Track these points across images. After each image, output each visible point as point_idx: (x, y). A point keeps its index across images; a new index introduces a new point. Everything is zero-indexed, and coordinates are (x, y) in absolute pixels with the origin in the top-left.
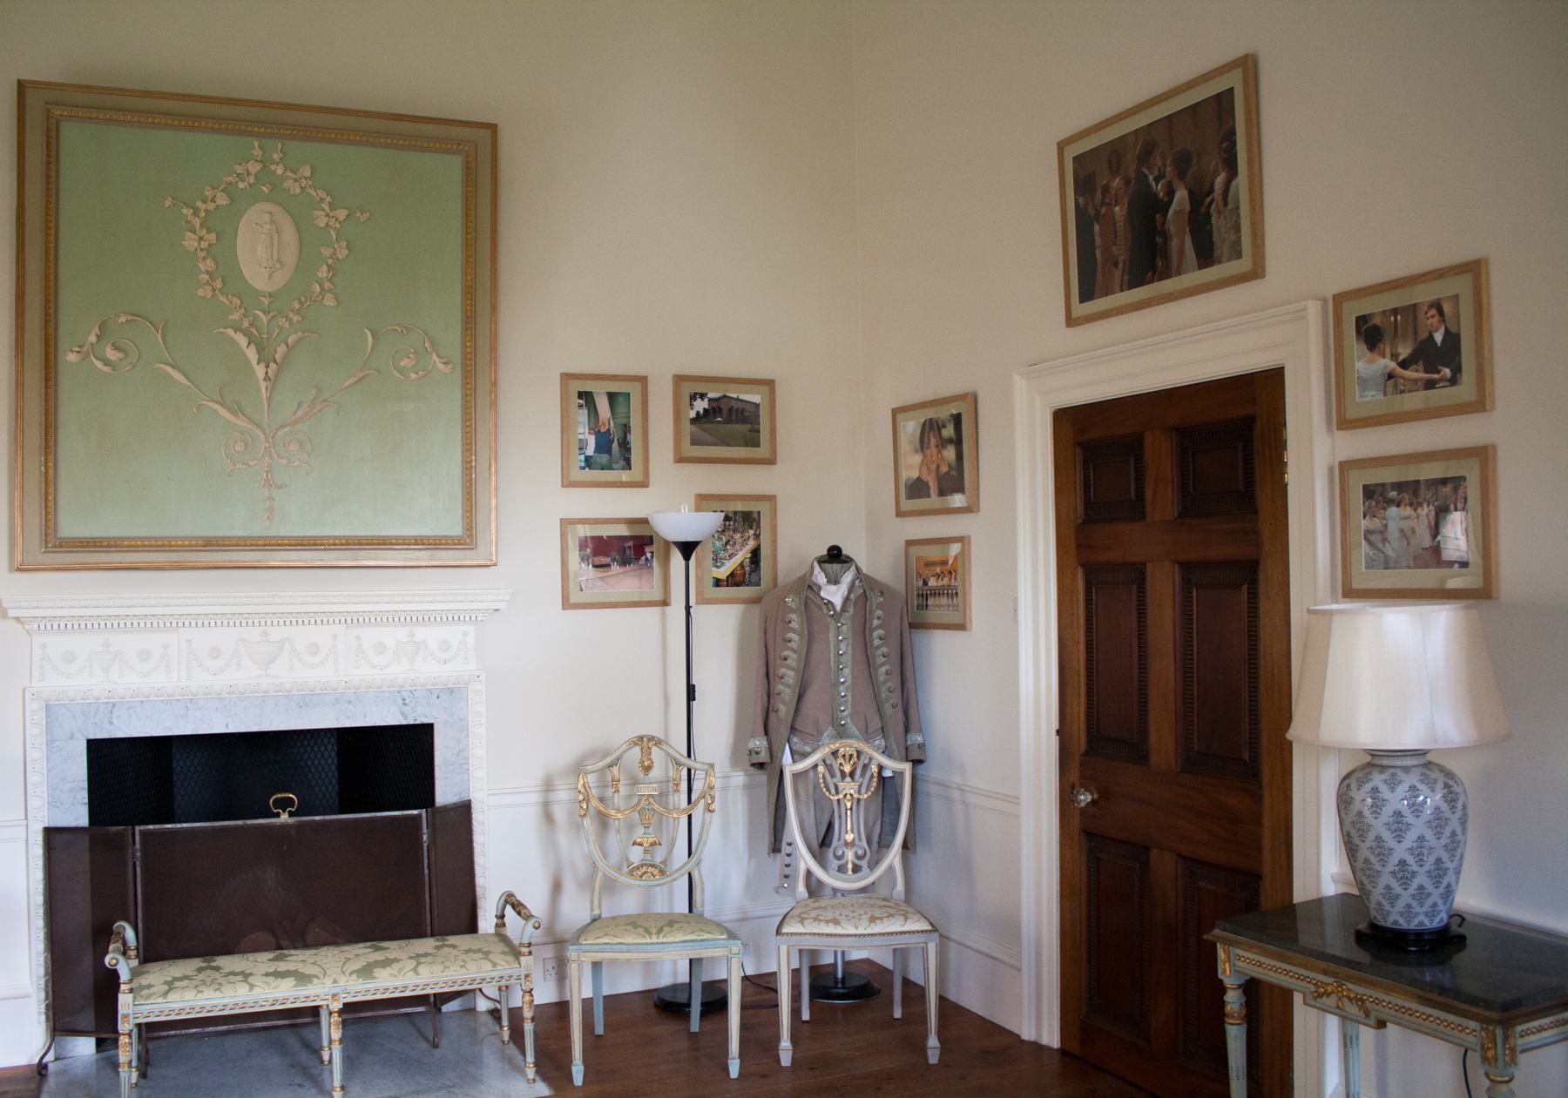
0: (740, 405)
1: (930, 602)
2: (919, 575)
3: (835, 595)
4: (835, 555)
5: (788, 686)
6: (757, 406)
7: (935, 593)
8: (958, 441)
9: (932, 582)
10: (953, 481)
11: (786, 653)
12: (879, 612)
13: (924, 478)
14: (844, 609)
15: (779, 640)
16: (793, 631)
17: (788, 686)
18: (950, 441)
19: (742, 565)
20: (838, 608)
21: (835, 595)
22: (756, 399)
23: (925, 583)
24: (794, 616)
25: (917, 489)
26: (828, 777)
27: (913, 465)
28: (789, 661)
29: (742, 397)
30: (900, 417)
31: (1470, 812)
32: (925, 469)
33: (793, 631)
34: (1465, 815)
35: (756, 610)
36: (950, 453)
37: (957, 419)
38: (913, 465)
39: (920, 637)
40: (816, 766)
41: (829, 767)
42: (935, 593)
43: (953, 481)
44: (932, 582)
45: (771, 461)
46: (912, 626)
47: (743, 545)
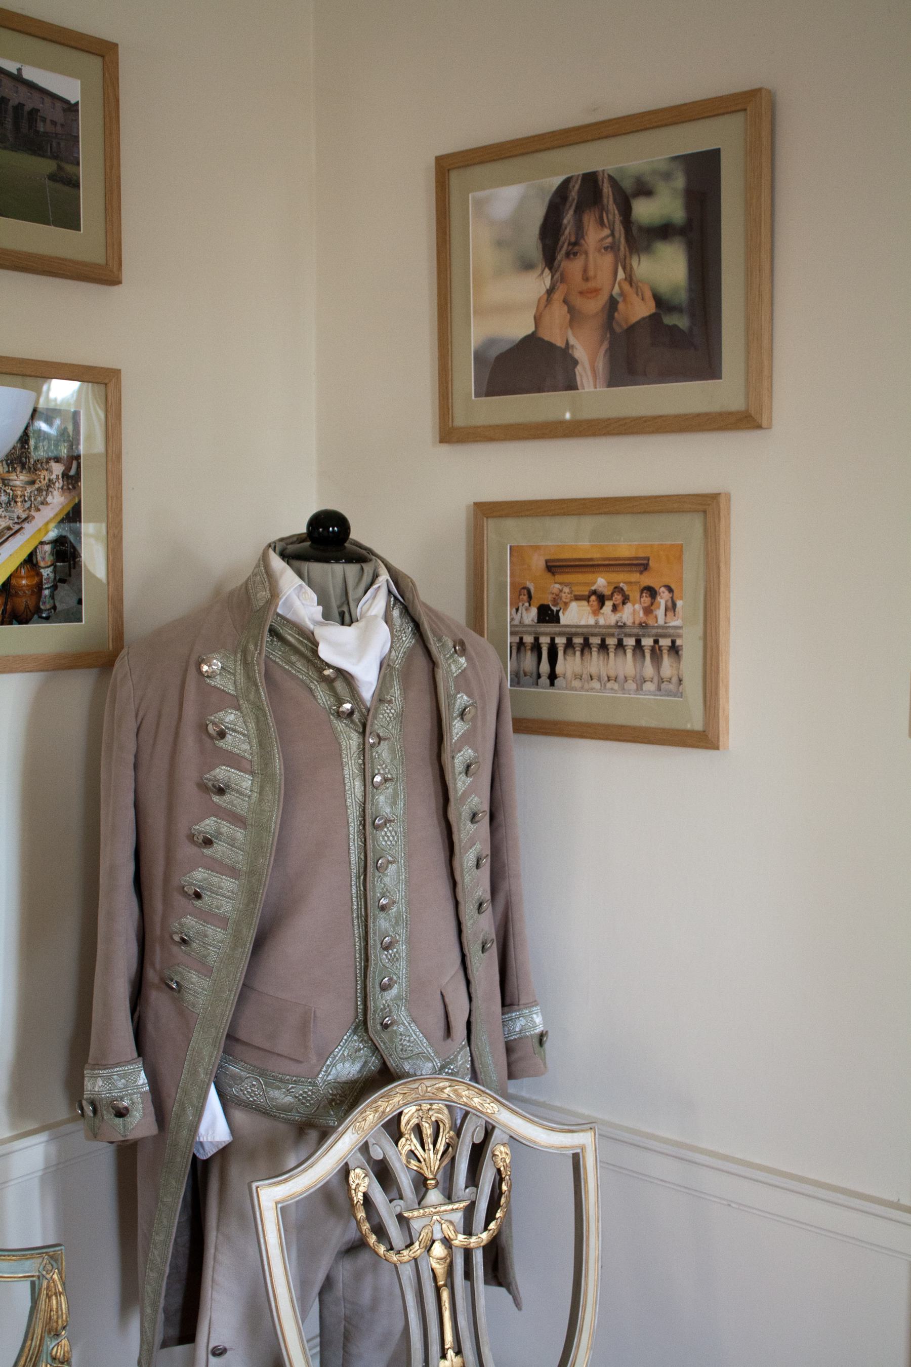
0: (31, 102)
1: (567, 665)
2: (524, 594)
3: (361, 650)
4: (326, 540)
5: (223, 921)
6: (71, 108)
7: (584, 643)
8: (699, 233)
9: (576, 615)
10: (677, 341)
11: (209, 825)
12: (462, 699)
13: (555, 335)
14: (381, 698)
15: (188, 789)
16: (234, 760)
17: (223, 921)
18: (664, 231)
19: (30, 561)
20: (367, 692)
21: (361, 650)
22: (68, 88)
23: (547, 615)
24: (230, 717)
25: (524, 366)
26: (379, 1197)
27: (510, 304)
28: (219, 849)
29: (31, 74)
30: (456, 179)
31: (133, 714)
32: (558, 312)
33: (234, 760)
34: (136, 717)
35: (78, 688)
36: (667, 267)
37: (702, 172)
38: (510, 304)
39: (539, 765)
40: (346, 1171)
41: (383, 1173)
42: (584, 643)
43: (677, 341)
44: (576, 615)
45: (105, 274)
46: (524, 726)
47: (35, 504)
